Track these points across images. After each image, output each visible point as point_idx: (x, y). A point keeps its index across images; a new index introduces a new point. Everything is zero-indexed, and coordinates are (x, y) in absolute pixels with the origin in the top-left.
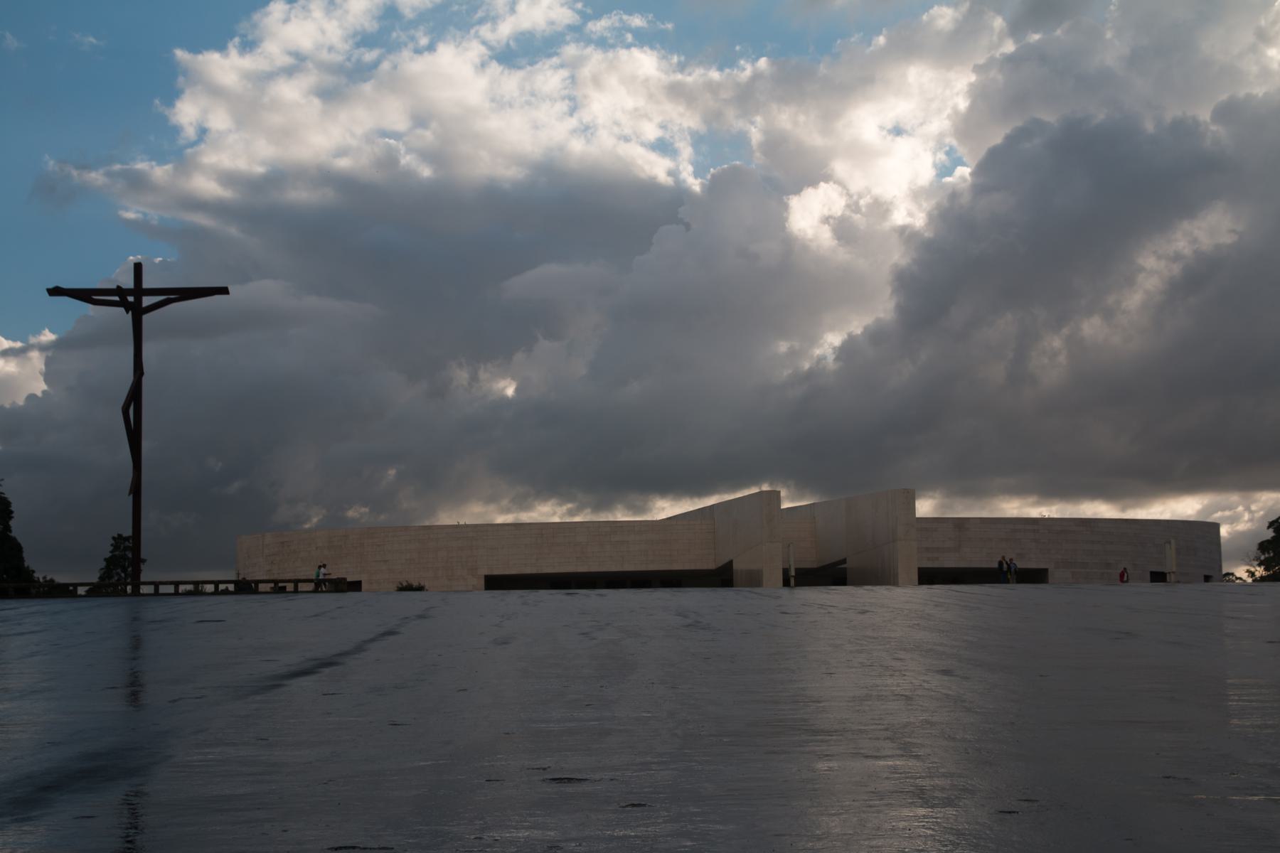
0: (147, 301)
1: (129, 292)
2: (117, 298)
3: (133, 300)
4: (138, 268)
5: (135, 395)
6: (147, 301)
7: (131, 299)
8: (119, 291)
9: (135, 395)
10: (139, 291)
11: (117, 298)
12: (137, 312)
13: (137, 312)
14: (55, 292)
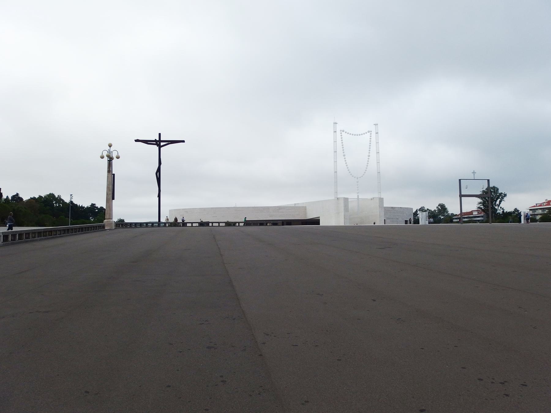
3: (158, 143)
4: (160, 134)
5: (159, 170)
6: (162, 144)
8: (155, 141)
9: (159, 170)
10: (160, 141)
12: (160, 147)
13: (160, 147)
14: (137, 141)
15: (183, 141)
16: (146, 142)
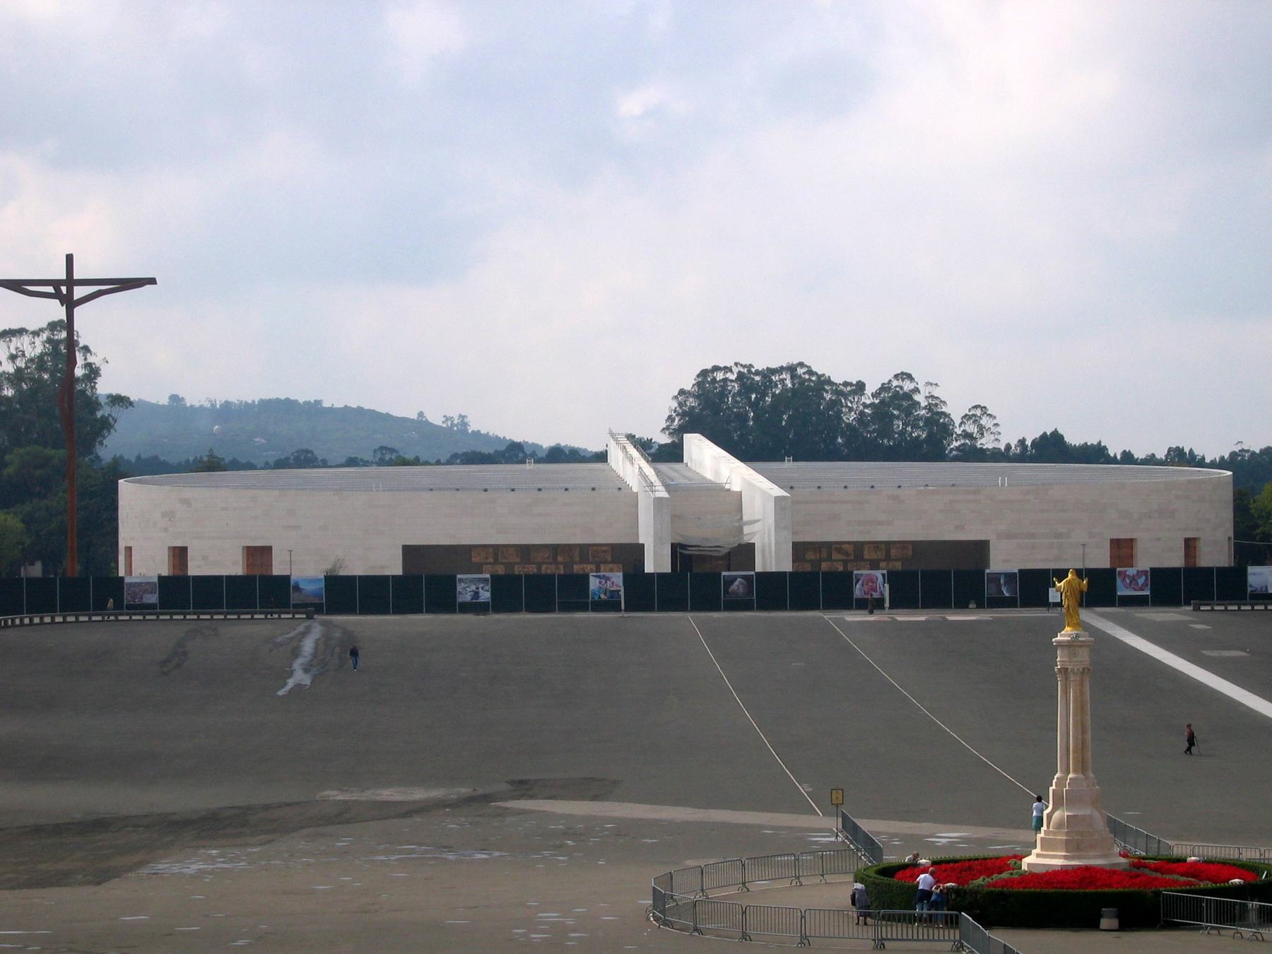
0: (79, 292)
2: (50, 289)
3: (65, 290)
4: (70, 258)
6: (79, 292)
8: (56, 283)
10: (71, 282)
11: (50, 289)
12: (70, 304)
15: (152, 281)
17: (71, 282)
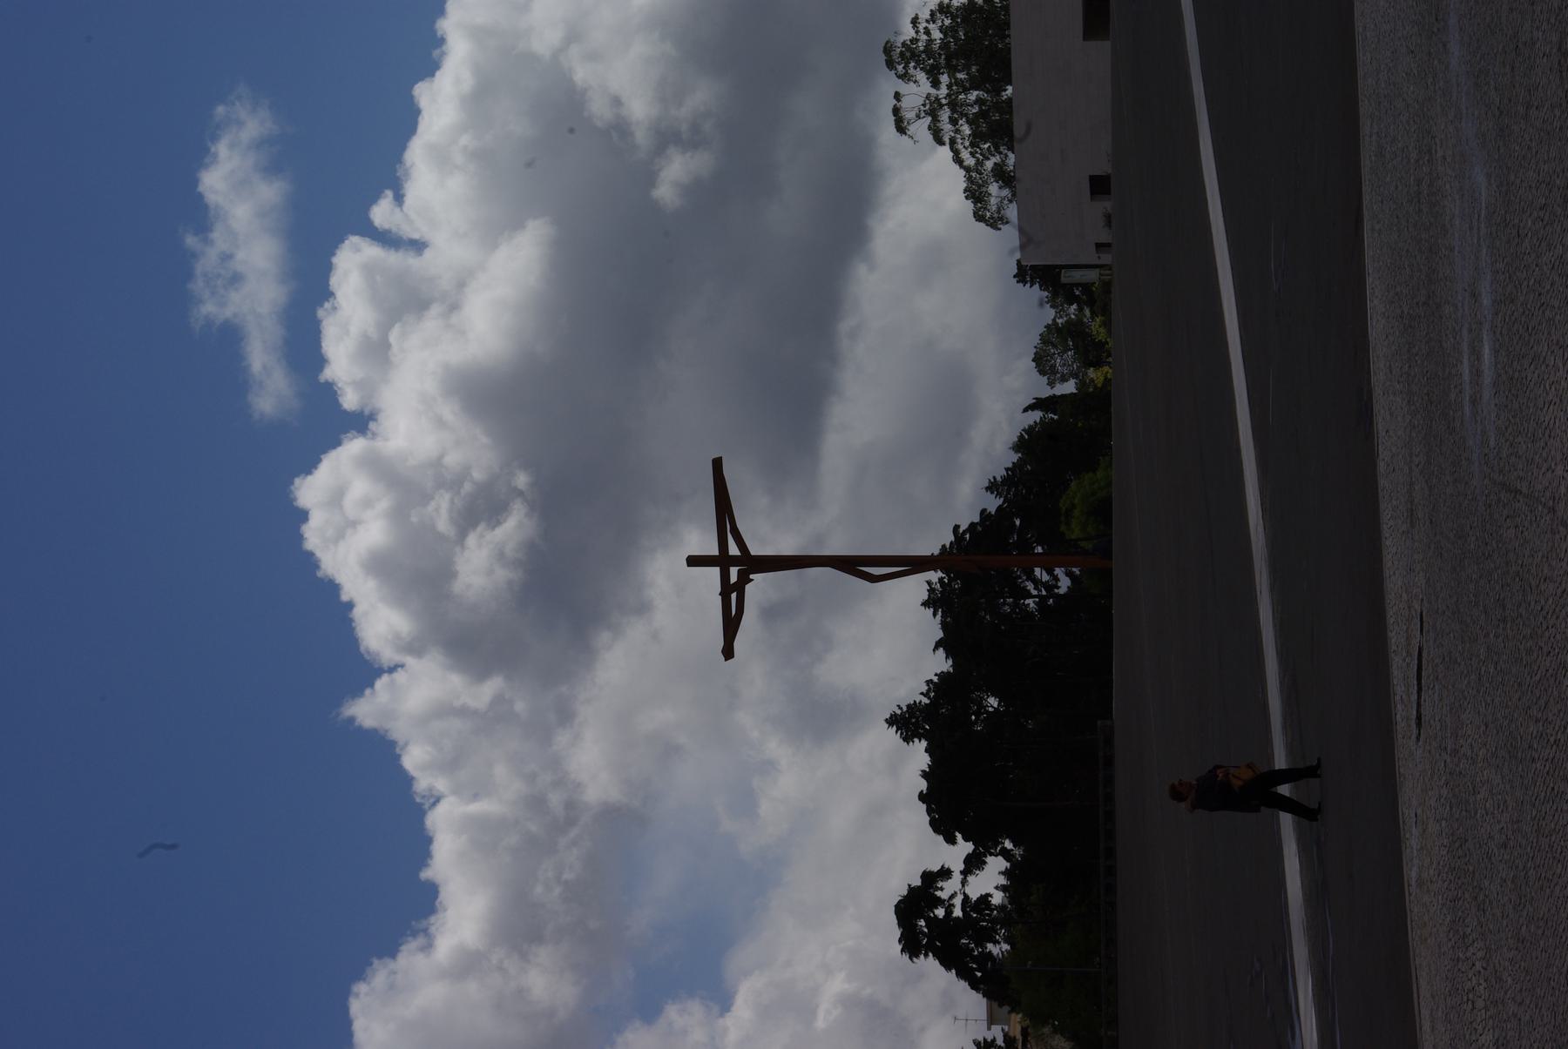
0: (734, 550)
1: (725, 576)
2: (734, 596)
4: (693, 561)
5: (850, 565)
6: (734, 550)
7: (734, 572)
9: (850, 565)
11: (734, 596)
12: (755, 564)
14: (728, 652)
15: (717, 464)
16: (731, 625)
17: (722, 561)
